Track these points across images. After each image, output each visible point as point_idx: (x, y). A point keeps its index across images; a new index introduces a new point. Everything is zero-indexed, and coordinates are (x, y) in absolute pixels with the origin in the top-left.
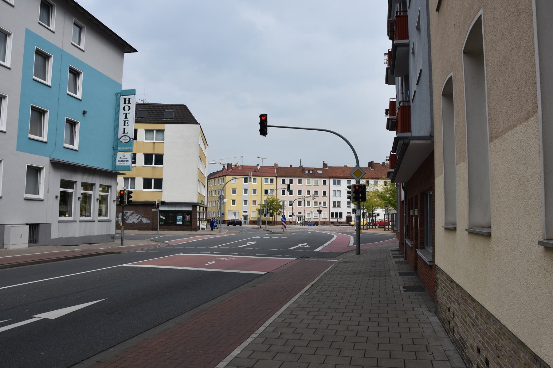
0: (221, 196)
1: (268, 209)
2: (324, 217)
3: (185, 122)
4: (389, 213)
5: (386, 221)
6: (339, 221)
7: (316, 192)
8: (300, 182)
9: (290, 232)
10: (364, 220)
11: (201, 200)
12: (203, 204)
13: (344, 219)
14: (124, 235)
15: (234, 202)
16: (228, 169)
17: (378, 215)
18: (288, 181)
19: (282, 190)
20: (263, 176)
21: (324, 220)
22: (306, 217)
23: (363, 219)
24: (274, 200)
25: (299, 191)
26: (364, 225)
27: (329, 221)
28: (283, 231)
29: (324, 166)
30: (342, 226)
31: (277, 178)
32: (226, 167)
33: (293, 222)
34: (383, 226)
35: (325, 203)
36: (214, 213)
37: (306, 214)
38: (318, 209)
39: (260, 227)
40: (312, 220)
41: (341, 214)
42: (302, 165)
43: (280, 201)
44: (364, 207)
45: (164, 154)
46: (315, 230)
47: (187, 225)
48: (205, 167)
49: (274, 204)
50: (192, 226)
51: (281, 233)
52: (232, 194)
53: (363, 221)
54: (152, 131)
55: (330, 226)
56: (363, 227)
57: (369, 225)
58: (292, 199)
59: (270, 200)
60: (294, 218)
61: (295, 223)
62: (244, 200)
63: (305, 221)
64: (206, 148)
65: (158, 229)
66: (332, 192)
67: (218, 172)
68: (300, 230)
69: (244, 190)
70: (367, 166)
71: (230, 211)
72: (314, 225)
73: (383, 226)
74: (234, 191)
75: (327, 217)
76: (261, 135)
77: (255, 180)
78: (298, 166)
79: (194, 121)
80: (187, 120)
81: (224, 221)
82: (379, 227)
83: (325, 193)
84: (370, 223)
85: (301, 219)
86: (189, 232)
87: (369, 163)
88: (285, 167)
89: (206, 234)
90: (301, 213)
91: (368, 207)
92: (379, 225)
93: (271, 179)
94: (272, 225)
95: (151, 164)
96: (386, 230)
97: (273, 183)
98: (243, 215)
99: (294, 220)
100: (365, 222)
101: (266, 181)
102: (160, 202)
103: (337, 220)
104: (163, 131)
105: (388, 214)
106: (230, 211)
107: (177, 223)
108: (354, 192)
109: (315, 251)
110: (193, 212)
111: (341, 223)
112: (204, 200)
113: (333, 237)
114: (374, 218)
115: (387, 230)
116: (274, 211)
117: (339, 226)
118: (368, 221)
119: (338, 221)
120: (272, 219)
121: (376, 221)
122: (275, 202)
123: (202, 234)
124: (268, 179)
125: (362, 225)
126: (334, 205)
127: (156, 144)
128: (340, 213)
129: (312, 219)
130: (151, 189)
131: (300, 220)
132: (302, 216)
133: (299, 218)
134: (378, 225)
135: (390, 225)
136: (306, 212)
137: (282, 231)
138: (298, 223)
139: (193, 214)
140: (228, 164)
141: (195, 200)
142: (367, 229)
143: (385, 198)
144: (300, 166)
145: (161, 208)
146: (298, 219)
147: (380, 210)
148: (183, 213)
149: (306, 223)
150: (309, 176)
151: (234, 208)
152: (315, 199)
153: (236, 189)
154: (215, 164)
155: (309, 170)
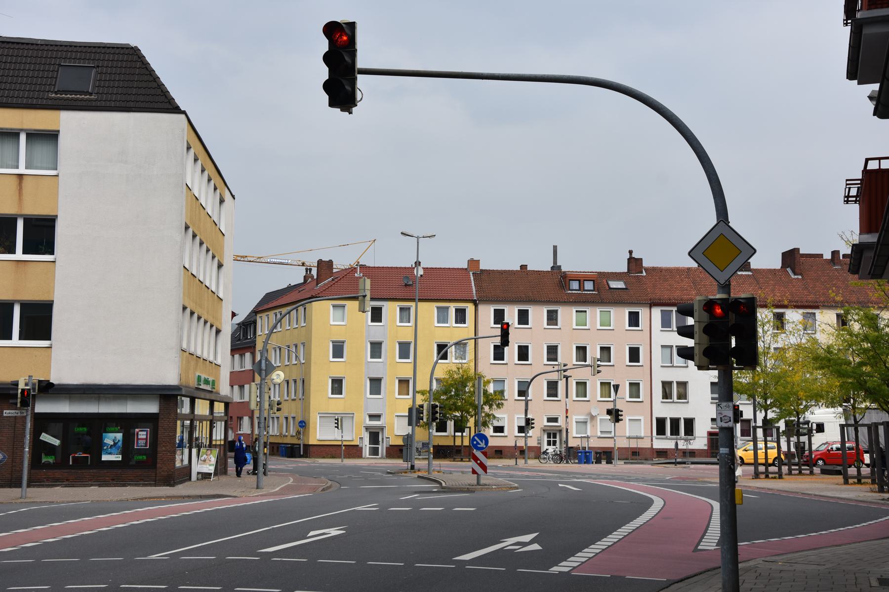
0: (263, 362)
1: (434, 407)
2: (634, 434)
3: (132, 104)
4: (861, 422)
5: (849, 449)
6: (685, 447)
7: (606, 350)
8: (552, 318)
9: (499, 487)
10: (770, 444)
11: (199, 377)
12: (211, 392)
13: (700, 442)
14: (427, 457)
15: (337, 385)
16: (318, 281)
17: (820, 428)
20: (421, 300)
21: (633, 444)
22: (573, 432)
23: (766, 442)
24: (468, 379)
25: (548, 347)
26: (770, 461)
27: (650, 446)
28: (478, 484)
29: (633, 265)
30: (693, 463)
31: (476, 305)
32: (314, 272)
33: (531, 448)
34: (839, 468)
35: (635, 387)
37: (574, 424)
38: (610, 406)
39: (413, 467)
40: (595, 443)
41: (690, 424)
42: (558, 264)
43: (489, 382)
44: (768, 403)
45: (57, 216)
46: (598, 476)
47: (140, 465)
48: (220, 266)
49: (467, 389)
50: (155, 467)
51: (468, 491)
52: (332, 359)
53: (766, 448)
54: (13, 135)
55: (652, 464)
56: (767, 469)
57: (786, 461)
58: (525, 373)
59: (456, 376)
60: (535, 437)
61: (538, 453)
62: (372, 380)
63: (570, 445)
64: (222, 201)
65: (343, 456)
66: (657, 352)
67: (290, 289)
68: (544, 477)
70: (777, 264)
71: (324, 416)
72: (598, 461)
73: (839, 468)
74: (338, 350)
75: (642, 435)
76: (332, 104)
77: (405, 314)
78: (547, 266)
79: (169, 106)
80: (142, 98)
81: (307, 446)
82: (824, 472)
83: (634, 355)
84: (789, 454)
85: (558, 439)
86: (144, 488)
87: (784, 254)
88: (505, 271)
89: (201, 497)
90: (555, 420)
91: (782, 401)
92: (825, 464)
93: (456, 310)
94: (462, 460)
95: (12, 251)
96: (851, 481)
97: (463, 321)
98: (367, 428)
99: (532, 443)
100: (773, 454)
101: (442, 315)
102: (34, 384)
103: (677, 444)
104: (52, 136)
105: (856, 425)
106: (324, 416)
107: (105, 458)
108: (707, 330)
109: (555, 569)
110: (161, 417)
111: (692, 453)
112: (218, 375)
113: (650, 502)
114: (803, 439)
115: (855, 483)
116: (468, 412)
117: (684, 463)
118: (784, 448)
119: (680, 447)
120: (460, 439)
121: (814, 448)
122: (470, 384)
123: (184, 497)
124: (447, 308)
125: (763, 461)
126: (666, 395)
127: (27, 183)
128: (672, 419)
129: (591, 440)
130: (10, 338)
131: (554, 443)
132: (560, 431)
133: (549, 437)
134: (820, 462)
135: (863, 463)
136: (574, 418)
137: (475, 482)
138: (545, 453)
139: (162, 423)
140: (320, 262)
141: (169, 377)
142: (780, 477)
143: (844, 367)
144: (552, 268)
145: (43, 407)
146: (546, 439)
147: (824, 410)
148: (127, 423)
149: (572, 454)
150: (582, 300)
151: (338, 404)
152: (599, 372)
153: (343, 342)
154: (287, 264)
155: (581, 279)
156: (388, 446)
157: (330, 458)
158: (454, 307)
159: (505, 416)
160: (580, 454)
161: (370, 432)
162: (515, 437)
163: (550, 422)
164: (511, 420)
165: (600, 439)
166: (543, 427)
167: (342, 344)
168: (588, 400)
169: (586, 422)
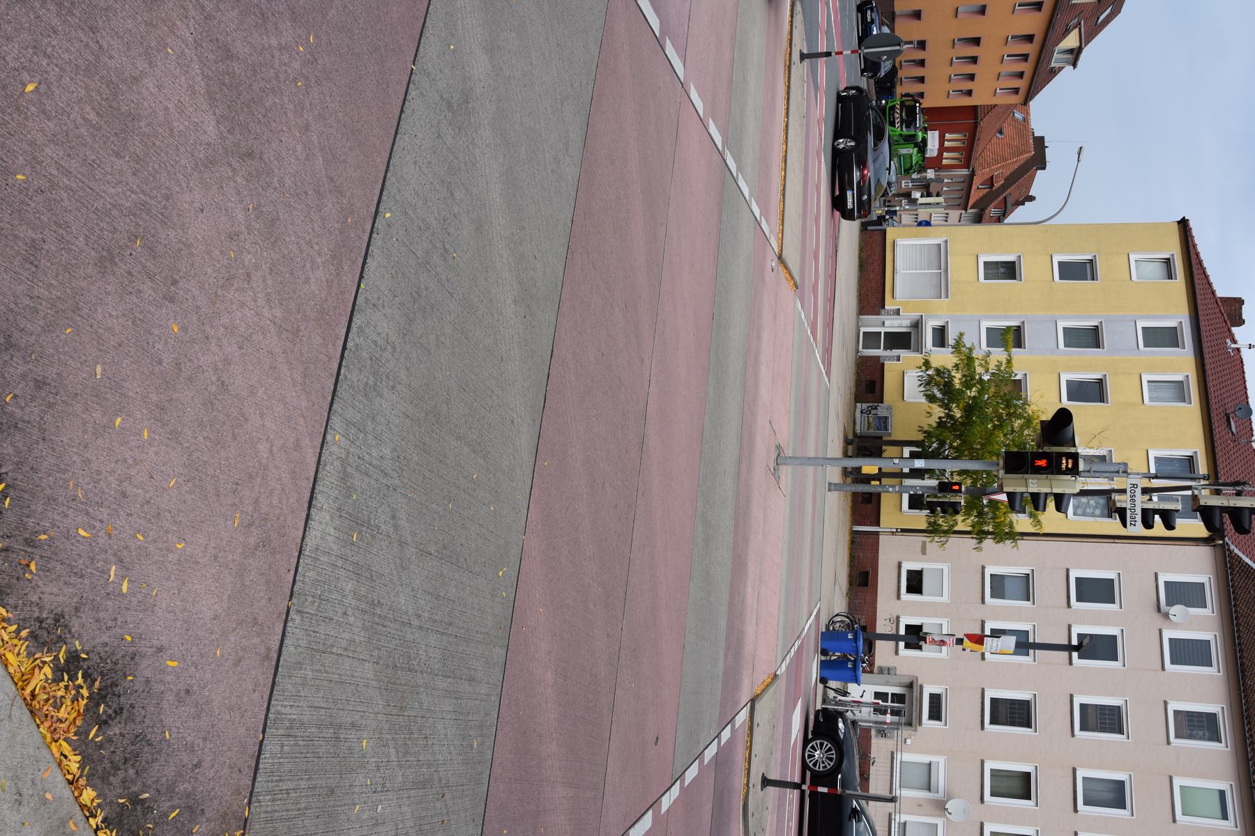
15: (915, 583)
18: (1191, 624)
19: (1114, 637)
36: (914, 215)
69: (1093, 323)
90: (936, 714)
98: (917, 325)
133: (898, 698)
156: (881, 361)
157: (860, 258)
158: (1196, 452)
159: (945, 598)
160: (850, 636)
161: (909, 333)
162: (898, 618)
163: (931, 702)
164: (935, 610)
165: (887, 818)
166: (920, 682)
167: (1089, 275)
168: (985, 799)
169: (929, 789)
